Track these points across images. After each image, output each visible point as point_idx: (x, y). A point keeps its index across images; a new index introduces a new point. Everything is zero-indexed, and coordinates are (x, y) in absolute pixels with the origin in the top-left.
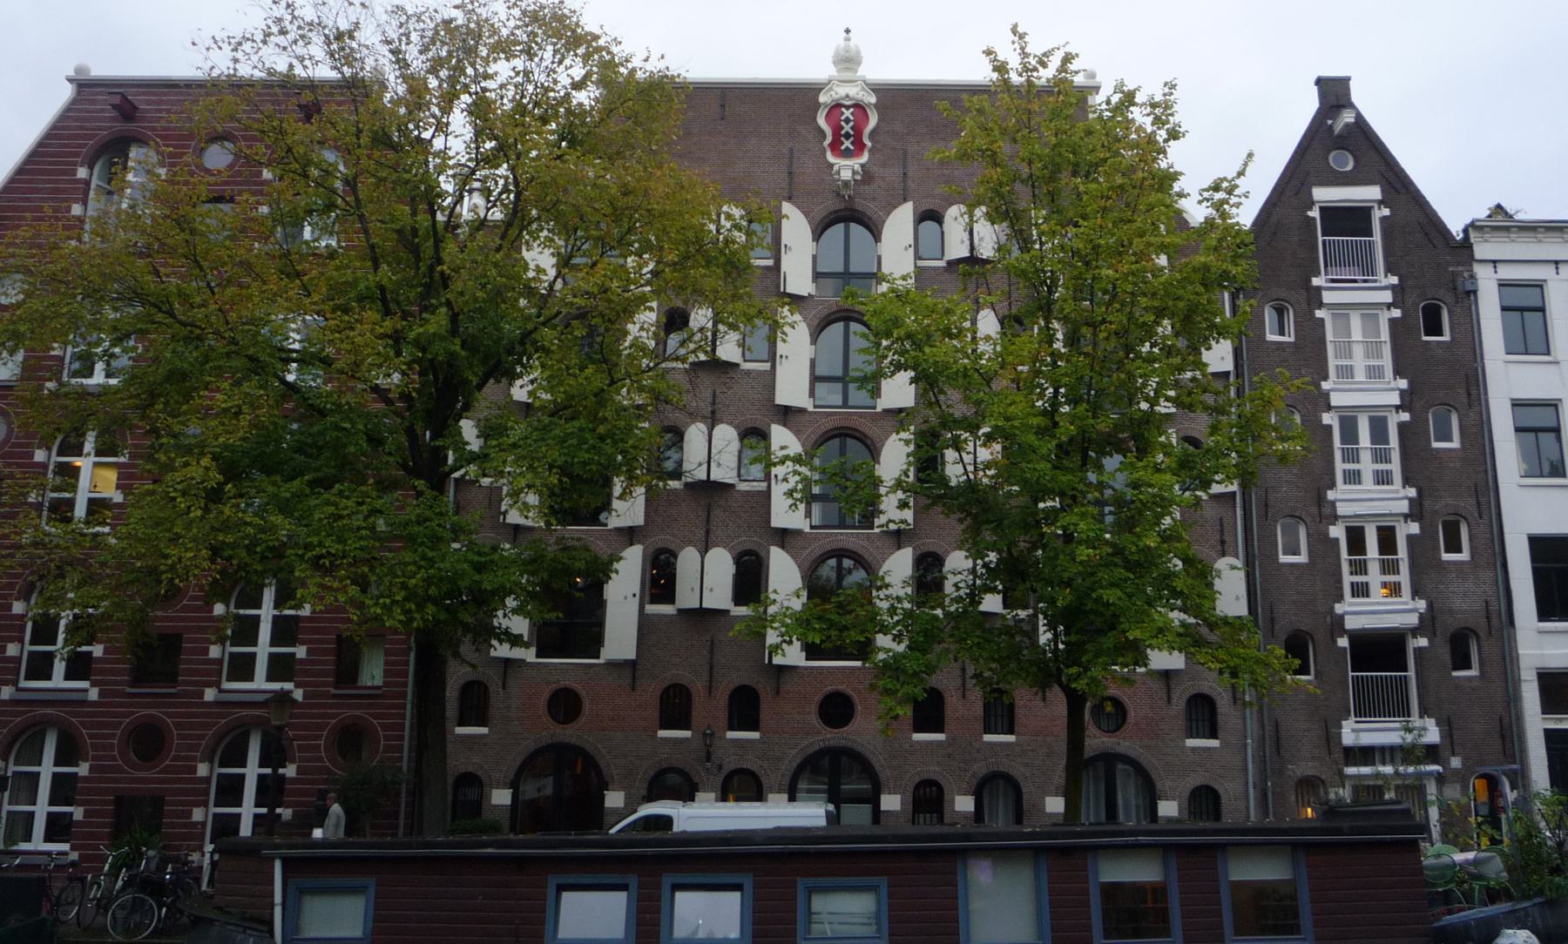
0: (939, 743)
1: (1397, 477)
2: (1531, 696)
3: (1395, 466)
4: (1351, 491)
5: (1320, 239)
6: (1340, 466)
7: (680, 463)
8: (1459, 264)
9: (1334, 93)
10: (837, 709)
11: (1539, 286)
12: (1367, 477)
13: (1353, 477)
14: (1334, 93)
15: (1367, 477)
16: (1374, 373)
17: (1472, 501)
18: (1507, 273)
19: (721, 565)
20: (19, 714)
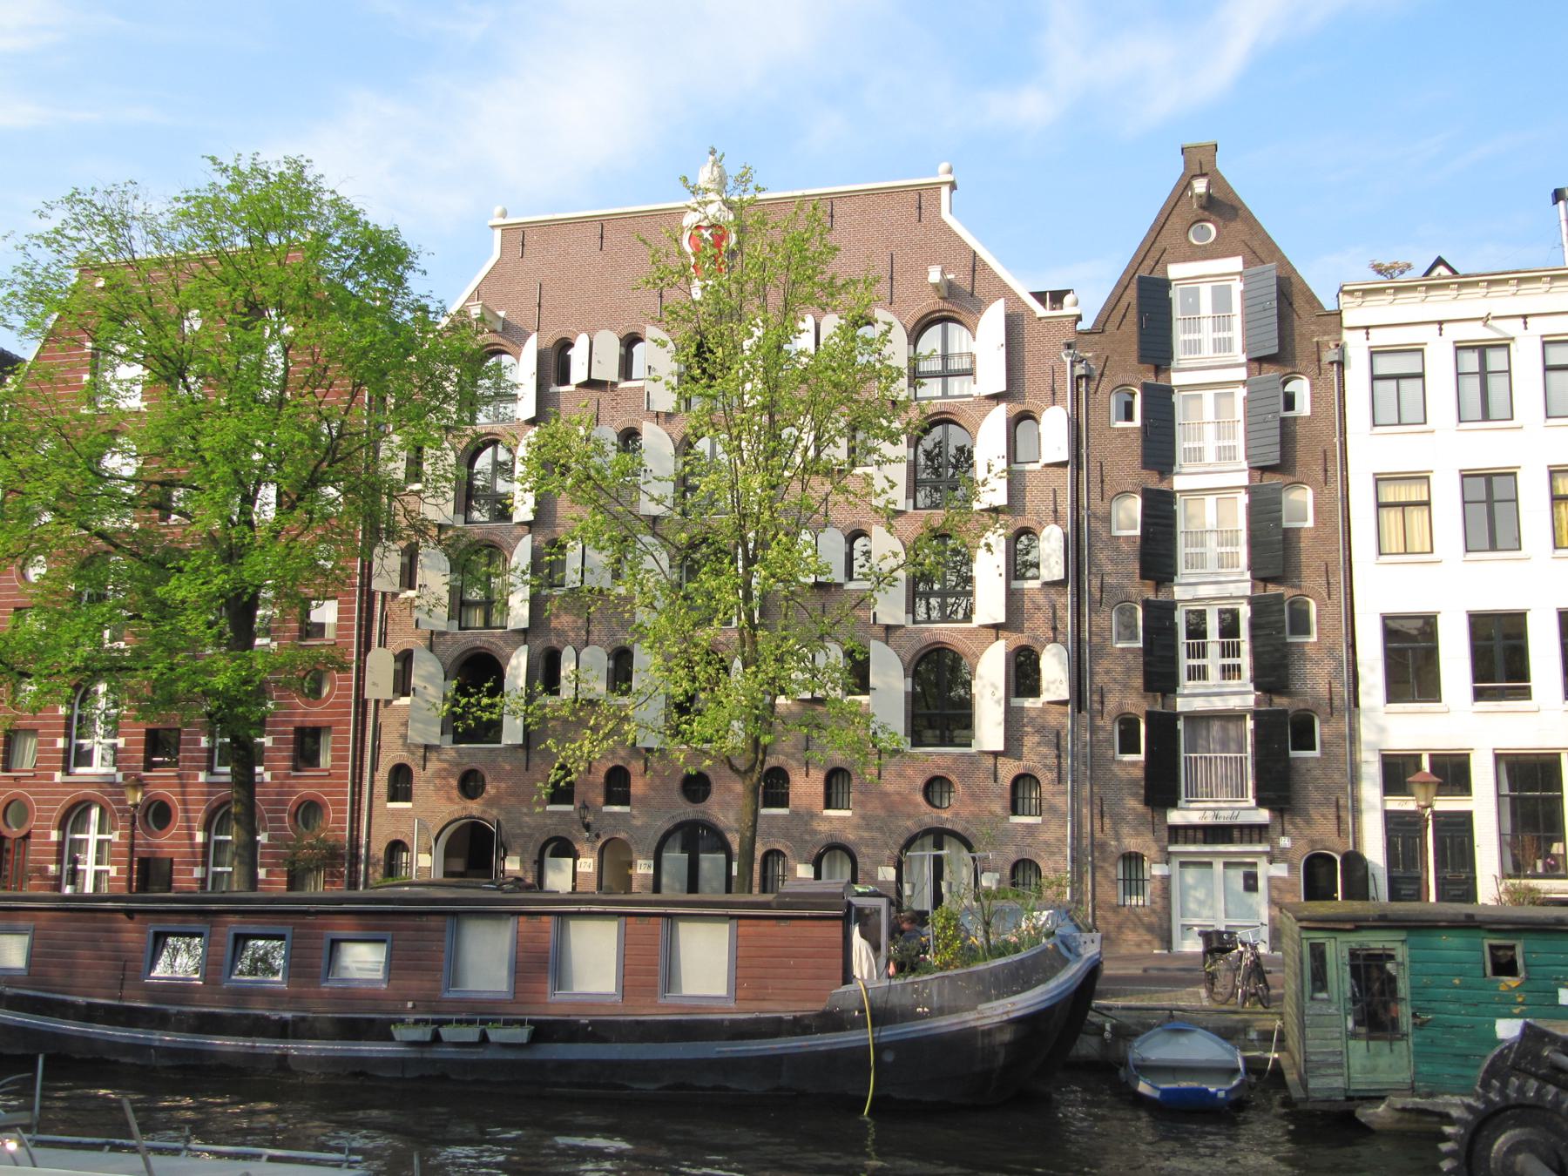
0: (784, 817)
1: (1247, 672)
2: (1371, 771)
3: (1245, 661)
4: (1195, 687)
5: (1183, 755)
6: (1184, 662)
7: (563, 578)
8: (1325, 333)
9: (1199, 160)
10: (696, 786)
11: (1418, 350)
12: (1214, 673)
13: (1199, 673)
14: (1199, 160)
15: (1214, 673)
16: (1224, 453)
17: (1323, 581)
18: (1380, 338)
19: (597, 660)
20: (68, 794)
